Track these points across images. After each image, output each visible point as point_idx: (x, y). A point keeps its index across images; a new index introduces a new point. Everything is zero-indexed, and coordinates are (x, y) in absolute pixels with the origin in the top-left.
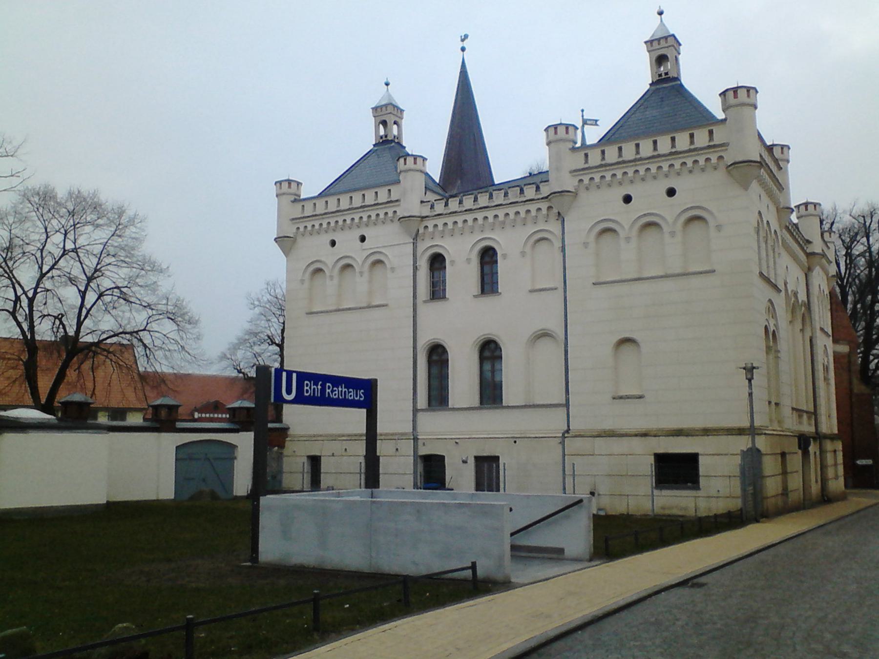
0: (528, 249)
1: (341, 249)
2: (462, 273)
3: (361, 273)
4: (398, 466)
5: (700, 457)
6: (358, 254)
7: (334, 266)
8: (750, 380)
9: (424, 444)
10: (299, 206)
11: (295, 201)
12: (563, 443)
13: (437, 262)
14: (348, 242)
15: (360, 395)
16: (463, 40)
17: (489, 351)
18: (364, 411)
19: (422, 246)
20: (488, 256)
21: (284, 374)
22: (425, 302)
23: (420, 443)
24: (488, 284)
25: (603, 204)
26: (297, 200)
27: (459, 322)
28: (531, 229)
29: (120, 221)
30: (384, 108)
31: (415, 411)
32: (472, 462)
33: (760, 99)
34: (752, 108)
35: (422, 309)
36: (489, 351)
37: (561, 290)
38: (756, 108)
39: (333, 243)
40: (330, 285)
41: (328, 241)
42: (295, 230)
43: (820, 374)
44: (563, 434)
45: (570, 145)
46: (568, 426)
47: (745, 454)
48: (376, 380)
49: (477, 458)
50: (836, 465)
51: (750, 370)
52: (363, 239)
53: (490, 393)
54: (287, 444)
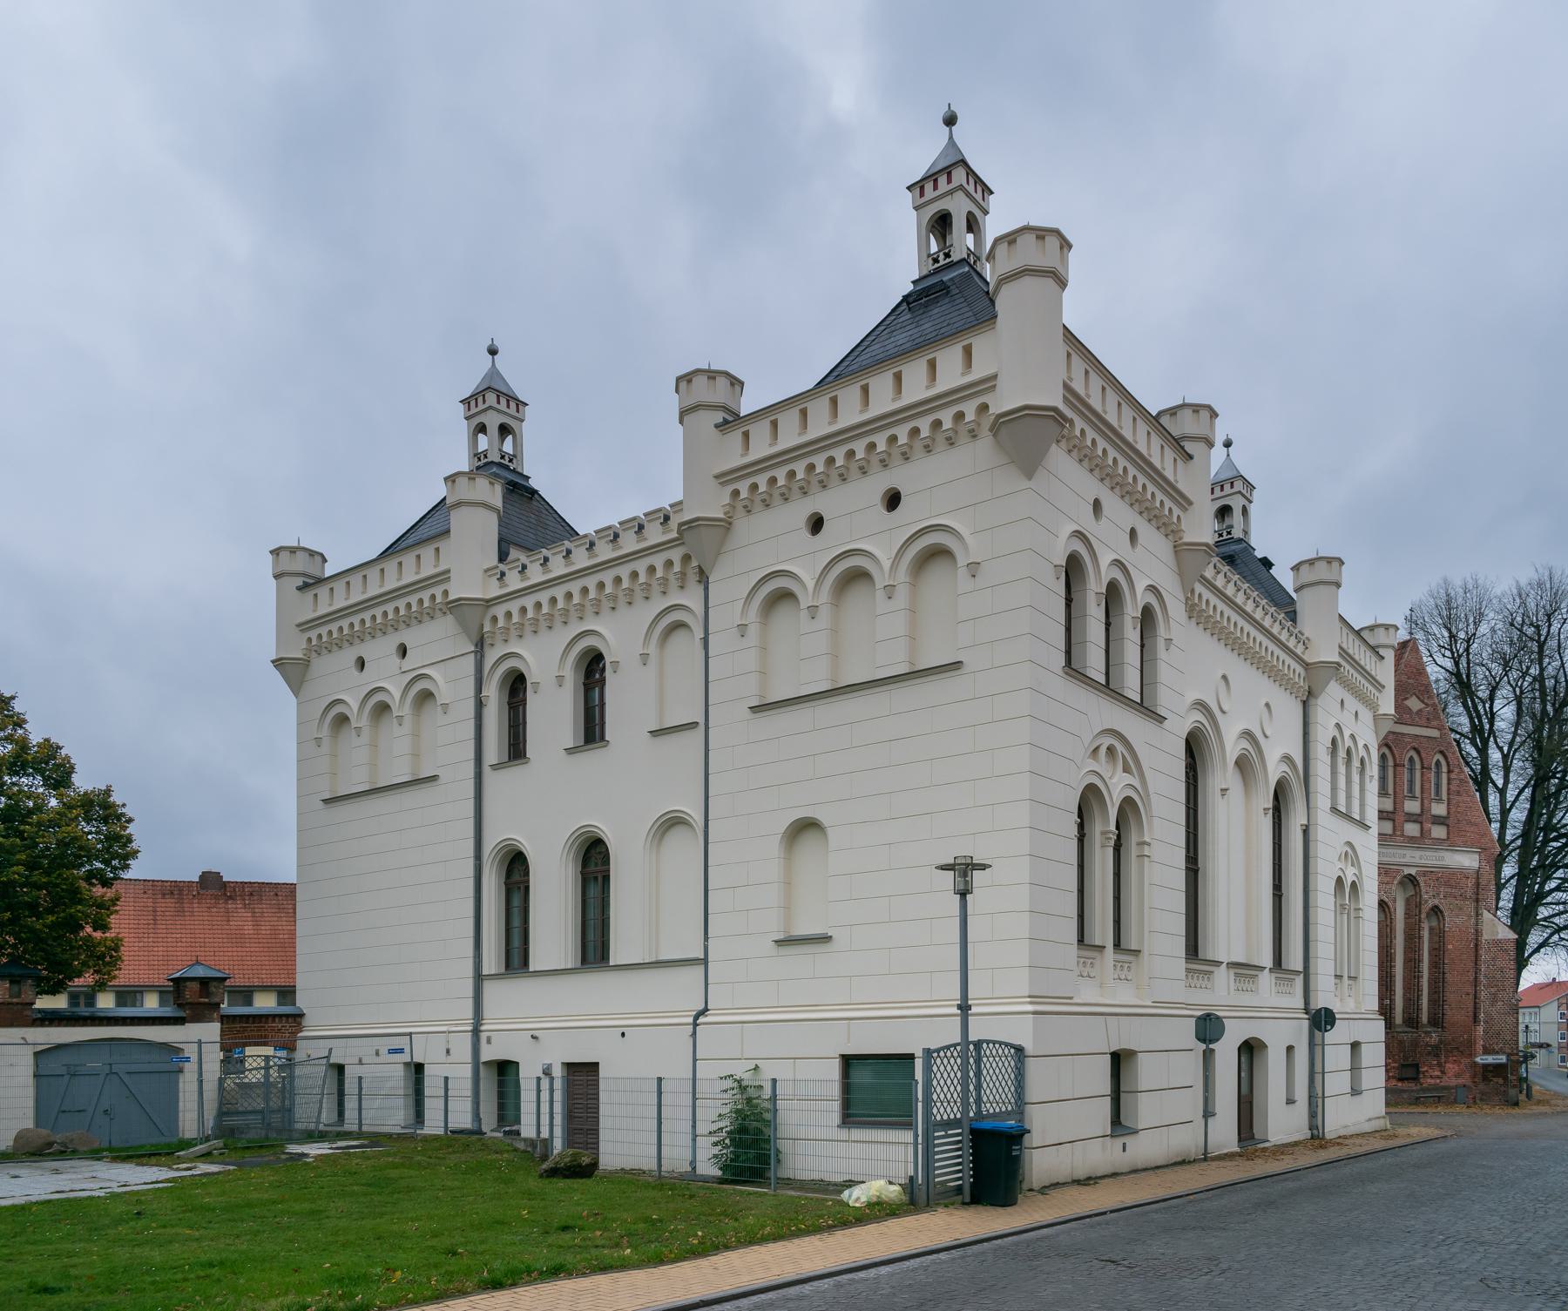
0: (652, 649)
2: (553, 712)
3: (890, 590)
7: (820, 581)
8: (963, 894)
9: (489, 1041)
10: (736, 436)
11: (723, 426)
13: (516, 685)
14: (854, 513)
17: (593, 858)
19: (491, 656)
20: (593, 667)
21: (1418, 794)
22: (495, 767)
23: (484, 1036)
24: (593, 730)
25: (773, 542)
26: (731, 420)
30: (943, 180)
31: (479, 978)
32: (558, 1072)
33: (1076, 266)
34: (1050, 282)
36: (593, 858)
37: (702, 727)
38: (1063, 284)
40: (356, 748)
41: (354, 658)
42: (727, 500)
44: (696, 1017)
45: (719, 417)
52: (403, 651)
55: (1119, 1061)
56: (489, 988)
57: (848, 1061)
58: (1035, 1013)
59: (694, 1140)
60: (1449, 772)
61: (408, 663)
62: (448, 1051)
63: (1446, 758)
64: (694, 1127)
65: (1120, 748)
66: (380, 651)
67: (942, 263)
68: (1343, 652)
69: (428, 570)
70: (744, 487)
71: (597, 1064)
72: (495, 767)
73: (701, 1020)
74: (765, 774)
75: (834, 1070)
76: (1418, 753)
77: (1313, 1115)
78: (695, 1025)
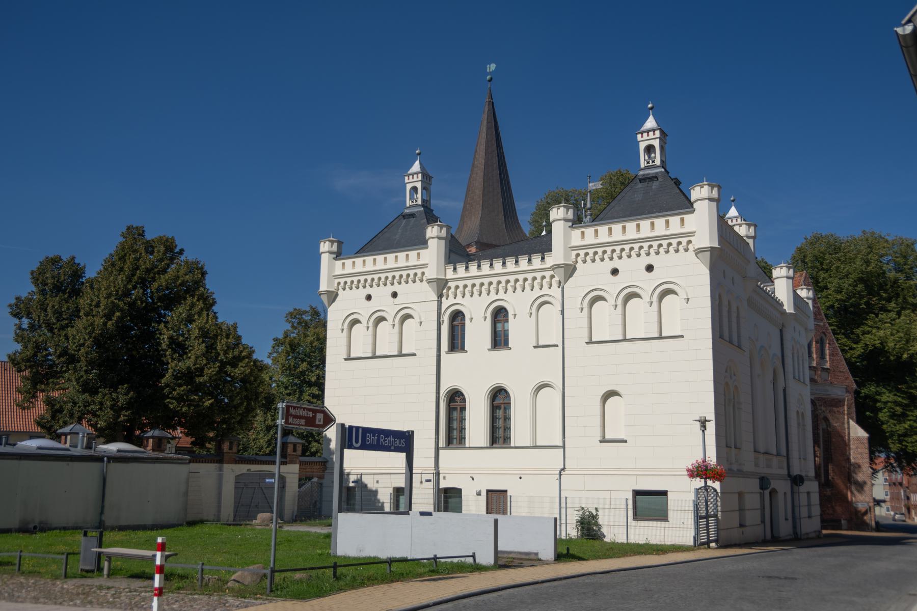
2: (478, 331)
4: (423, 497)
6: (390, 309)
9: (444, 478)
13: (457, 317)
15: (403, 443)
16: (430, 514)
17: (499, 399)
18: (404, 454)
19: (445, 303)
20: (500, 315)
23: (441, 477)
24: (499, 340)
28: (537, 292)
31: (437, 449)
32: (484, 493)
35: (443, 355)
36: (499, 399)
37: (560, 347)
39: (369, 298)
43: (793, 423)
47: (697, 491)
48: (413, 432)
49: (488, 491)
50: (809, 505)
51: (703, 423)
53: (499, 435)
56: (441, 451)
57: (637, 493)
61: (397, 300)
66: (381, 294)
73: (563, 473)
74: (590, 371)
75: (630, 496)
77: (794, 527)
78: (560, 475)
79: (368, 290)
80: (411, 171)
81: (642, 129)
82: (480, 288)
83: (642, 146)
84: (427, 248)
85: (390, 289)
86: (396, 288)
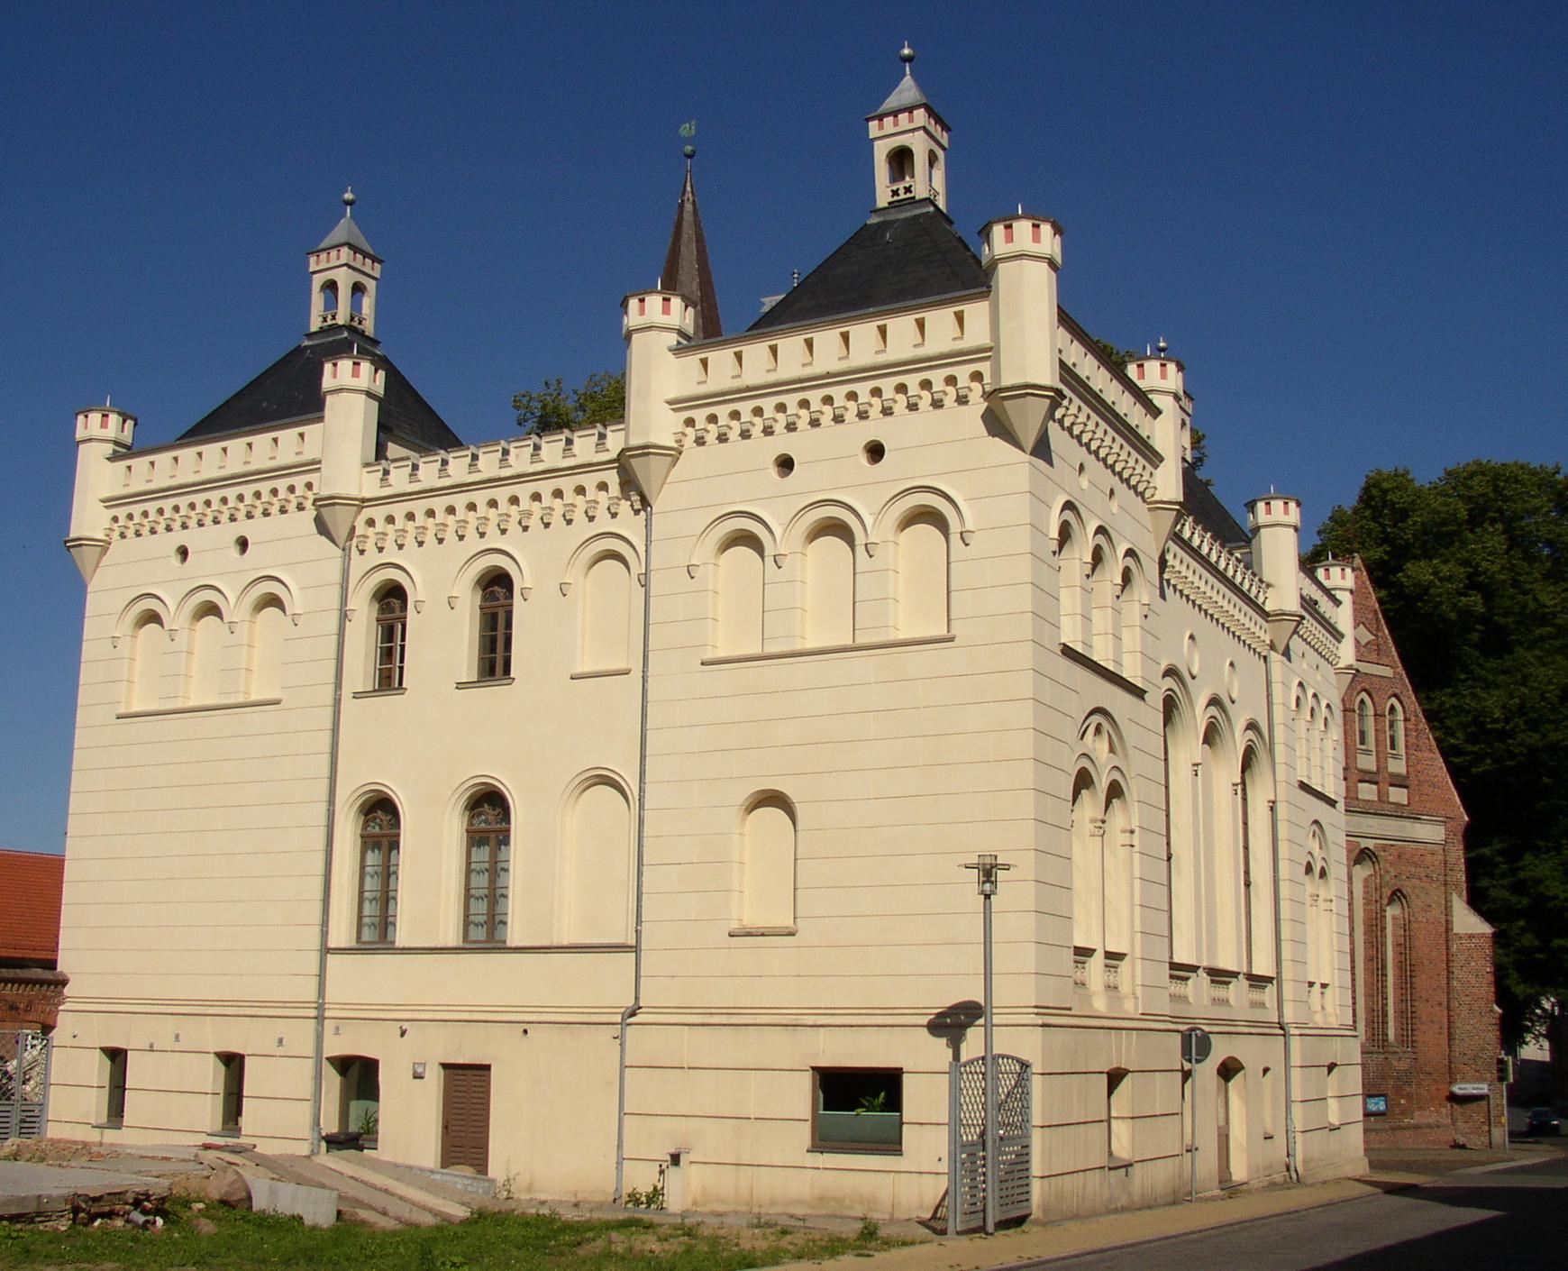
1: (200, 569)
5: (905, 1077)
6: (231, 579)
12: (621, 1038)
13: (392, 597)
17: (488, 809)
19: (359, 565)
20: (496, 585)
22: (357, 696)
24: (494, 660)
27: (429, 743)
29: (1480, 470)
31: (325, 950)
32: (435, 1078)
36: (488, 809)
37: (637, 674)
46: (637, 998)
53: (485, 927)
54: (62, 1019)
55: (233, 1063)
58: (1043, 1025)
59: (619, 1164)
60: (1406, 720)
62: (177, 1037)
63: (1401, 702)
64: (620, 1146)
65: (1106, 726)
66: (211, 543)
67: (902, 196)
68: (1066, 371)
69: (286, 456)
70: (700, 416)
71: (487, 1068)
72: (357, 696)
76: (1369, 694)
79: (179, 537)
80: (891, 102)
81: (882, 109)
82: (449, 522)
83: (881, 151)
84: (321, 419)
85: (231, 531)
86: (243, 527)
